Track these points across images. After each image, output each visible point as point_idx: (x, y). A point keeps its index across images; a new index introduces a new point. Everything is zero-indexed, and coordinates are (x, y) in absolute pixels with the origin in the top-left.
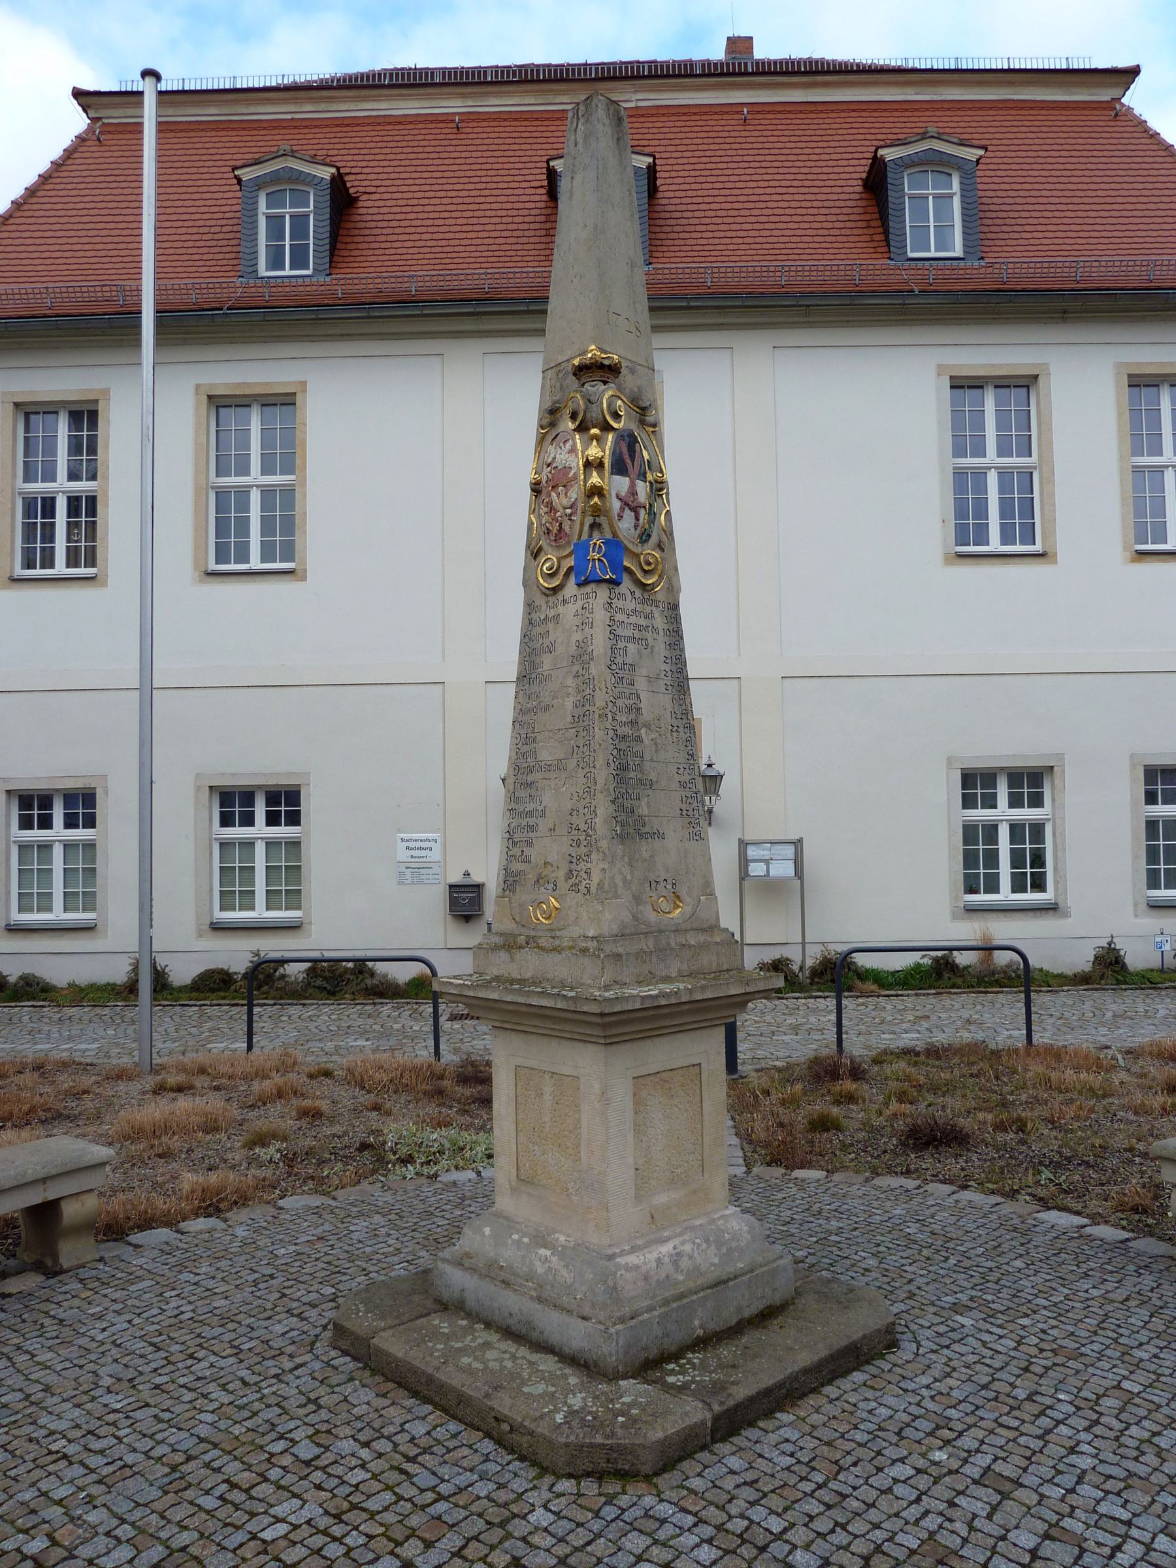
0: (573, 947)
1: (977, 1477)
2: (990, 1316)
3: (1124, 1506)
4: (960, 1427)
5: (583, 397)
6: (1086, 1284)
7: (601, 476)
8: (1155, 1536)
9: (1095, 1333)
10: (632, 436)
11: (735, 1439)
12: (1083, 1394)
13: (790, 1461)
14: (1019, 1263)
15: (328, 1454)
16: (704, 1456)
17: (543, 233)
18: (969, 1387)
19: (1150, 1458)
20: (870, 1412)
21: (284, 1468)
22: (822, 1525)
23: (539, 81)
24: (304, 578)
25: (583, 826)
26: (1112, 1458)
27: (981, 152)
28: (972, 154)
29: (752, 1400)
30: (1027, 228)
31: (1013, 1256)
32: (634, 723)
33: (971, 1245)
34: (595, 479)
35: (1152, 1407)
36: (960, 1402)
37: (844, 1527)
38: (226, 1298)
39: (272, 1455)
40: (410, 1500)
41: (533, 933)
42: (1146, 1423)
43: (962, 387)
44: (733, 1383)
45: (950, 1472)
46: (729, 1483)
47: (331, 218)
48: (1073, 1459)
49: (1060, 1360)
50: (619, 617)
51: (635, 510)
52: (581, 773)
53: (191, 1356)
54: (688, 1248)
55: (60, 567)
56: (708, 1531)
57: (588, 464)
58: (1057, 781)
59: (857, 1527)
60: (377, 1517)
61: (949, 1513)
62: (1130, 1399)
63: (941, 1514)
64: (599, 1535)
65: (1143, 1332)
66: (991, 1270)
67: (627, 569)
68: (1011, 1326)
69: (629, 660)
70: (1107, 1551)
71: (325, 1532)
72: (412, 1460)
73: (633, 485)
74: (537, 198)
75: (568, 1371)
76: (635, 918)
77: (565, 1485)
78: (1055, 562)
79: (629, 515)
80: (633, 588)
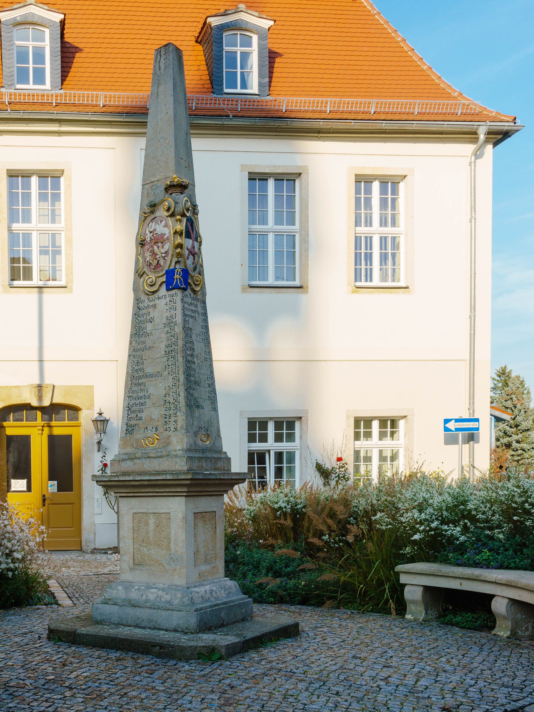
10: (191, 219)
27: (272, 23)
32: (192, 355)
50: (186, 306)
51: (194, 255)
52: (171, 377)
54: (214, 588)
55: (376, 281)
57: (176, 233)
69: (190, 326)
73: (193, 244)
79: (191, 257)
80: (191, 293)
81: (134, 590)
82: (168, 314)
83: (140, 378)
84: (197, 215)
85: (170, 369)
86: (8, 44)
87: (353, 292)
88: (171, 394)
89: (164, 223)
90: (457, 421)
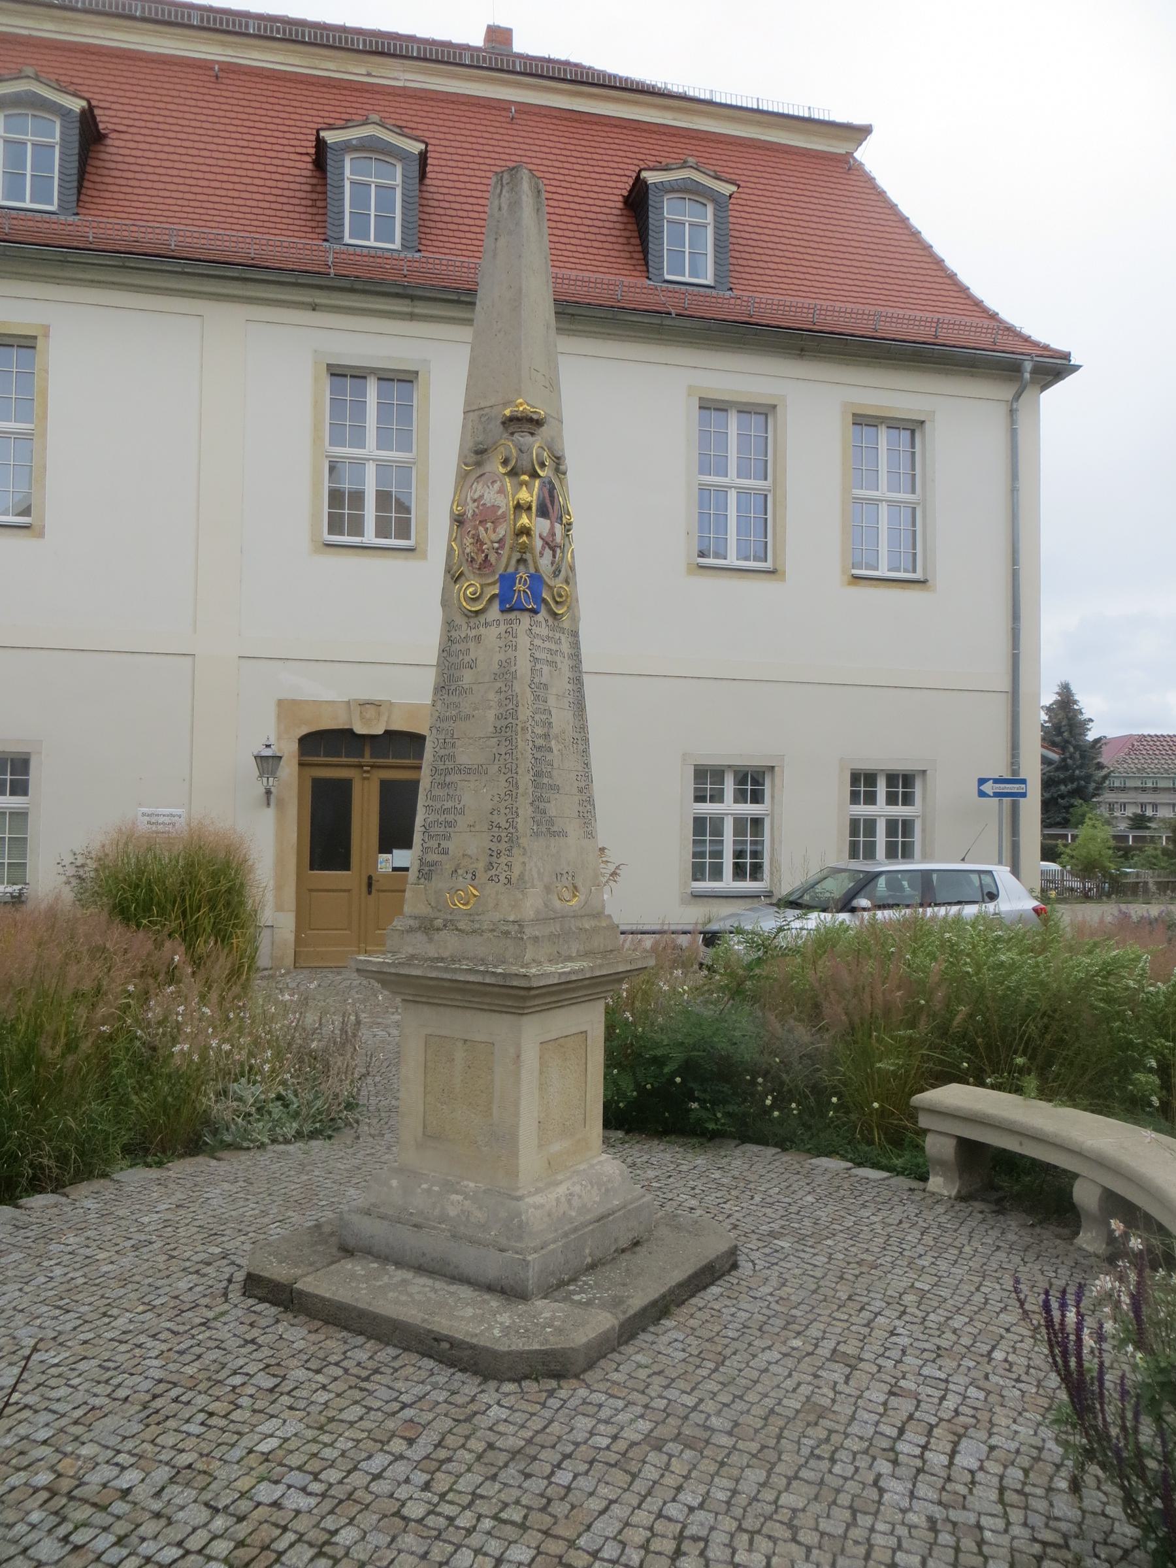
0: (493, 930)
1: (828, 1356)
2: (802, 1239)
3: (940, 1369)
4: (805, 1322)
5: (515, 446)
6: (865, 1213)
7: (530, 518)
8: (967, 1388)
9: (884, 1248)
10: (551, 482)
11: (636, 1342)
12: (889, 1293)
13: (682, 1355)
14: (810, 1198)
15: (286, 1382)
16: (615, 1356)
17: (309, 203)
18: (803, 1293)
19: (949, 1335)
20: (732, 1315)
21: (251, 1396)
22: (725, 1398)
23: (303, 43)
24: (41, 535)
25: (504, 824)
26: (921, 1337)
27: (734, 188)
28: (727, 189)
29: (644, 1310)
30: (771, 265)
31: (803, 1193)
32: (546, 736)
33: (768, 1186)
34: (524, 520)
35: (941, 1299)
36: (799, 1304)
37: (741, 1398)
38: (112, 1263)
39: (234, 1387)
40: (378, 1409)
41: (450, 917)
42: (940, 1311)
43: (709, 408)
44: (628, 1297)
45: (808, 1354)
46: (642, 1374)
47: (79, 154)
48: (894, 1339)
49: (864, 1269)
50: (537, 642)
52: (503, 778)
53: (105, 1315)
54: (577, 1189)
55: (370, 536)
56: (639, 1410)
58: (777, 781)
59: (751, 1397)
60: (356, 1425)
61: (816, 1382)
62: (923, 1294)
63: (809, 1384)
64: (551, 1421)
65: (920, 1246)
66: (790, 1204)
67: (544, 600)
68: (820, 1247)
69: (543, 680)
70: (936, 1401)
71: (315, 1440)
72: (367, 1379)
73: (552, 527)
74: (303, 165)
75: (487, 1297)
76: (546, 905)
77: (509, 1387)
78: (783, 580)
79: (548, 553)
81: (419, 1190)
82: (502, 656)
83: (448, 772)
84: (564, 473)
85: (502, 761)
86: (336, 178)
87: (850, 584)
88: (503, 811)
89: (497, 486)
90: (996, 781)
